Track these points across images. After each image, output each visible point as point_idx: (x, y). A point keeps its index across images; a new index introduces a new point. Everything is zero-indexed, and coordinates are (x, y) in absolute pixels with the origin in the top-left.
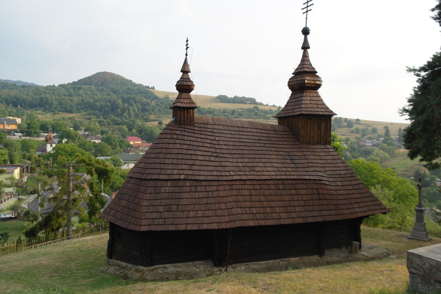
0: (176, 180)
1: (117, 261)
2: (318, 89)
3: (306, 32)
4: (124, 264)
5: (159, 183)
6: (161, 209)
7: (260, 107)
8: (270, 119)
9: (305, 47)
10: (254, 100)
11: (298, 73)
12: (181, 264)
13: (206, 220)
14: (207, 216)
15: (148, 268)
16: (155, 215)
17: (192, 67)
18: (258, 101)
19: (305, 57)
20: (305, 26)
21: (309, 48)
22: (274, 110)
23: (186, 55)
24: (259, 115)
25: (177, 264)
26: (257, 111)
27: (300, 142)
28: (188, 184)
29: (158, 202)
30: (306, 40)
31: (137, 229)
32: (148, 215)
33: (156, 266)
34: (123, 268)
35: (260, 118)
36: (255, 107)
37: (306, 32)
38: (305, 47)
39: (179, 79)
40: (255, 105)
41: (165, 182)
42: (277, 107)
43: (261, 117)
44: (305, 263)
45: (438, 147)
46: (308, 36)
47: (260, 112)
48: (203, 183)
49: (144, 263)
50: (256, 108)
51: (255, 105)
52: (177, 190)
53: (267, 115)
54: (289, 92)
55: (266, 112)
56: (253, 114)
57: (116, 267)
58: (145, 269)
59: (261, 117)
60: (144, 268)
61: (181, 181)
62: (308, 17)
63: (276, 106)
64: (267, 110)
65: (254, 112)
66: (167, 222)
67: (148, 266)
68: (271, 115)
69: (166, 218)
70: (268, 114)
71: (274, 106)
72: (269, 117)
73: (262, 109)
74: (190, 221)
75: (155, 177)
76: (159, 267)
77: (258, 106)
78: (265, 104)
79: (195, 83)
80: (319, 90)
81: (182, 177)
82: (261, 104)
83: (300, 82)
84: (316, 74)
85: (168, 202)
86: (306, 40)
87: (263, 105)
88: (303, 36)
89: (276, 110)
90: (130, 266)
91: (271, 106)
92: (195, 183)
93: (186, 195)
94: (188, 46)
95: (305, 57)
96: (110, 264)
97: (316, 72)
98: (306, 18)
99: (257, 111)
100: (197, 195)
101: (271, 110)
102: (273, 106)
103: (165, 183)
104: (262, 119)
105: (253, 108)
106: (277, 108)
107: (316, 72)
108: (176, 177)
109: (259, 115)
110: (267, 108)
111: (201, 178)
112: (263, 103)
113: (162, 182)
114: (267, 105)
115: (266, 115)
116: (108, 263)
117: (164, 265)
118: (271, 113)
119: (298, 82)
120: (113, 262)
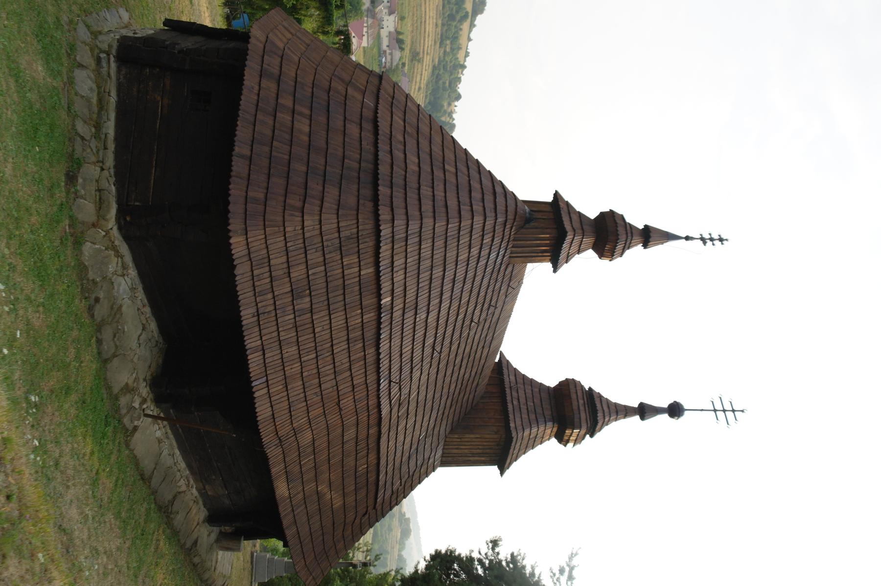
0: (379, 288)
1: (114, 93)
2: (556, 437)
3: (675, 410)
4: (110, 128)
5: (367, 245)
6: (298, 272)
7: (465, 26)
8: (440, 47)
9: (644, 411)
10: (481, 11)
11: (591, 396)
12: (141, 294)
13: (277, 388)
14: (289, 387)
15: (115, 232)
16: (278, 261)
17: (657, 251)
18: (479, 19)
19: (624, 411)
20: (686, 408)
21: (642, 418)
22: (459, 56)
23: (687, 238)
24: (449, 23)
25: (140, 288)
26: (458, 18)
27: (450, 433)
28: (370, 316)
29: (315, 257)
30: (657, 411)
31: (235, 224)
32: (277, 243)
33: (124, 249)
34: (98, 126)
35: (443, 25)
36: (467, 13)
37: (675, 410)
38: (644, 411)
39: (628, 220)
40: (470, 14)
41: (371, 260)
42: (465, 61)
43: (446, 28)
44: (189, 514)
45: (338, 36)
46: (666, 416)
47: (456, 27)
48: (371, 351)
49: (128, 219)
50: (465, 17)
51: (470, 14)
52: (352, 297)
53: (448, 42)
54: (551, 382)
55: (455, 38)
56: (452, 9)
57: (94, 101)
58: (112, 223)
59: (446, 28)
60: (113, 219)
61: (375, 300)
62: (703, 412)
63: (467, 59)
64: (461, 42)
65: (457, 12)
66: (261, 298)
67: (120, 229)
68: (448, 50)
69: (273, 292)
70: (451, 43)
71: (467, 54)
72: (445, 47)
73: (461, 29)
74: (272, 355)
75: (385, 231)
76: (122, 257)
77: (469, 20)
78: (472, 35)
79: (618, 261)
80: (554, 441)
81: (386, 300)
82: (472, 25)
83: (576, 420)
84: (588, 436)
85: (319, 284)
86: (657, 411)
87: (470, 31)
88: (666, 406)
89: (459, 60)
90: (110, 162)
91: (467, 49)
92: (370, 334)
93: (338, 320)
94: (709, 243)
95: (624, 411)
96: (99, 60)
97: (592, 436)
98: (702, 410)
99: (458, 18)
100: (340, 347)
101: (459, 48)
102: (467, 52)
103: (368, 258)
104: (442, 30)
105: (465, 9)
106: (462, 63)
107: (592, 436)
108: (386, 286)
109: (449, 23)
110: (463, 40)
111: (384, 347)
112: (474, 30)
113: (371, 252)
114: (469, 39)
115: (448, 38)
116: (102, 51)
117: (131, 264)
118: (452, 49)
119: (576, 412)
120: (109, 75)
